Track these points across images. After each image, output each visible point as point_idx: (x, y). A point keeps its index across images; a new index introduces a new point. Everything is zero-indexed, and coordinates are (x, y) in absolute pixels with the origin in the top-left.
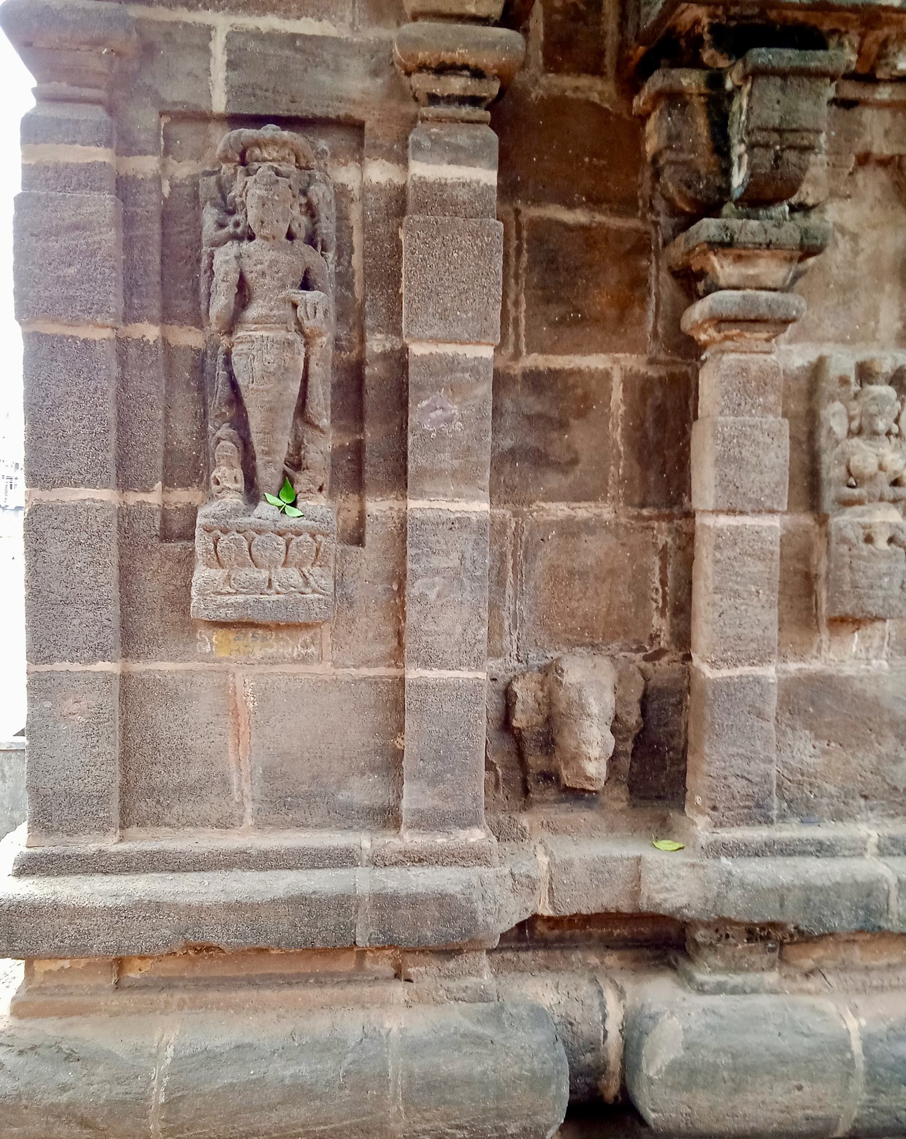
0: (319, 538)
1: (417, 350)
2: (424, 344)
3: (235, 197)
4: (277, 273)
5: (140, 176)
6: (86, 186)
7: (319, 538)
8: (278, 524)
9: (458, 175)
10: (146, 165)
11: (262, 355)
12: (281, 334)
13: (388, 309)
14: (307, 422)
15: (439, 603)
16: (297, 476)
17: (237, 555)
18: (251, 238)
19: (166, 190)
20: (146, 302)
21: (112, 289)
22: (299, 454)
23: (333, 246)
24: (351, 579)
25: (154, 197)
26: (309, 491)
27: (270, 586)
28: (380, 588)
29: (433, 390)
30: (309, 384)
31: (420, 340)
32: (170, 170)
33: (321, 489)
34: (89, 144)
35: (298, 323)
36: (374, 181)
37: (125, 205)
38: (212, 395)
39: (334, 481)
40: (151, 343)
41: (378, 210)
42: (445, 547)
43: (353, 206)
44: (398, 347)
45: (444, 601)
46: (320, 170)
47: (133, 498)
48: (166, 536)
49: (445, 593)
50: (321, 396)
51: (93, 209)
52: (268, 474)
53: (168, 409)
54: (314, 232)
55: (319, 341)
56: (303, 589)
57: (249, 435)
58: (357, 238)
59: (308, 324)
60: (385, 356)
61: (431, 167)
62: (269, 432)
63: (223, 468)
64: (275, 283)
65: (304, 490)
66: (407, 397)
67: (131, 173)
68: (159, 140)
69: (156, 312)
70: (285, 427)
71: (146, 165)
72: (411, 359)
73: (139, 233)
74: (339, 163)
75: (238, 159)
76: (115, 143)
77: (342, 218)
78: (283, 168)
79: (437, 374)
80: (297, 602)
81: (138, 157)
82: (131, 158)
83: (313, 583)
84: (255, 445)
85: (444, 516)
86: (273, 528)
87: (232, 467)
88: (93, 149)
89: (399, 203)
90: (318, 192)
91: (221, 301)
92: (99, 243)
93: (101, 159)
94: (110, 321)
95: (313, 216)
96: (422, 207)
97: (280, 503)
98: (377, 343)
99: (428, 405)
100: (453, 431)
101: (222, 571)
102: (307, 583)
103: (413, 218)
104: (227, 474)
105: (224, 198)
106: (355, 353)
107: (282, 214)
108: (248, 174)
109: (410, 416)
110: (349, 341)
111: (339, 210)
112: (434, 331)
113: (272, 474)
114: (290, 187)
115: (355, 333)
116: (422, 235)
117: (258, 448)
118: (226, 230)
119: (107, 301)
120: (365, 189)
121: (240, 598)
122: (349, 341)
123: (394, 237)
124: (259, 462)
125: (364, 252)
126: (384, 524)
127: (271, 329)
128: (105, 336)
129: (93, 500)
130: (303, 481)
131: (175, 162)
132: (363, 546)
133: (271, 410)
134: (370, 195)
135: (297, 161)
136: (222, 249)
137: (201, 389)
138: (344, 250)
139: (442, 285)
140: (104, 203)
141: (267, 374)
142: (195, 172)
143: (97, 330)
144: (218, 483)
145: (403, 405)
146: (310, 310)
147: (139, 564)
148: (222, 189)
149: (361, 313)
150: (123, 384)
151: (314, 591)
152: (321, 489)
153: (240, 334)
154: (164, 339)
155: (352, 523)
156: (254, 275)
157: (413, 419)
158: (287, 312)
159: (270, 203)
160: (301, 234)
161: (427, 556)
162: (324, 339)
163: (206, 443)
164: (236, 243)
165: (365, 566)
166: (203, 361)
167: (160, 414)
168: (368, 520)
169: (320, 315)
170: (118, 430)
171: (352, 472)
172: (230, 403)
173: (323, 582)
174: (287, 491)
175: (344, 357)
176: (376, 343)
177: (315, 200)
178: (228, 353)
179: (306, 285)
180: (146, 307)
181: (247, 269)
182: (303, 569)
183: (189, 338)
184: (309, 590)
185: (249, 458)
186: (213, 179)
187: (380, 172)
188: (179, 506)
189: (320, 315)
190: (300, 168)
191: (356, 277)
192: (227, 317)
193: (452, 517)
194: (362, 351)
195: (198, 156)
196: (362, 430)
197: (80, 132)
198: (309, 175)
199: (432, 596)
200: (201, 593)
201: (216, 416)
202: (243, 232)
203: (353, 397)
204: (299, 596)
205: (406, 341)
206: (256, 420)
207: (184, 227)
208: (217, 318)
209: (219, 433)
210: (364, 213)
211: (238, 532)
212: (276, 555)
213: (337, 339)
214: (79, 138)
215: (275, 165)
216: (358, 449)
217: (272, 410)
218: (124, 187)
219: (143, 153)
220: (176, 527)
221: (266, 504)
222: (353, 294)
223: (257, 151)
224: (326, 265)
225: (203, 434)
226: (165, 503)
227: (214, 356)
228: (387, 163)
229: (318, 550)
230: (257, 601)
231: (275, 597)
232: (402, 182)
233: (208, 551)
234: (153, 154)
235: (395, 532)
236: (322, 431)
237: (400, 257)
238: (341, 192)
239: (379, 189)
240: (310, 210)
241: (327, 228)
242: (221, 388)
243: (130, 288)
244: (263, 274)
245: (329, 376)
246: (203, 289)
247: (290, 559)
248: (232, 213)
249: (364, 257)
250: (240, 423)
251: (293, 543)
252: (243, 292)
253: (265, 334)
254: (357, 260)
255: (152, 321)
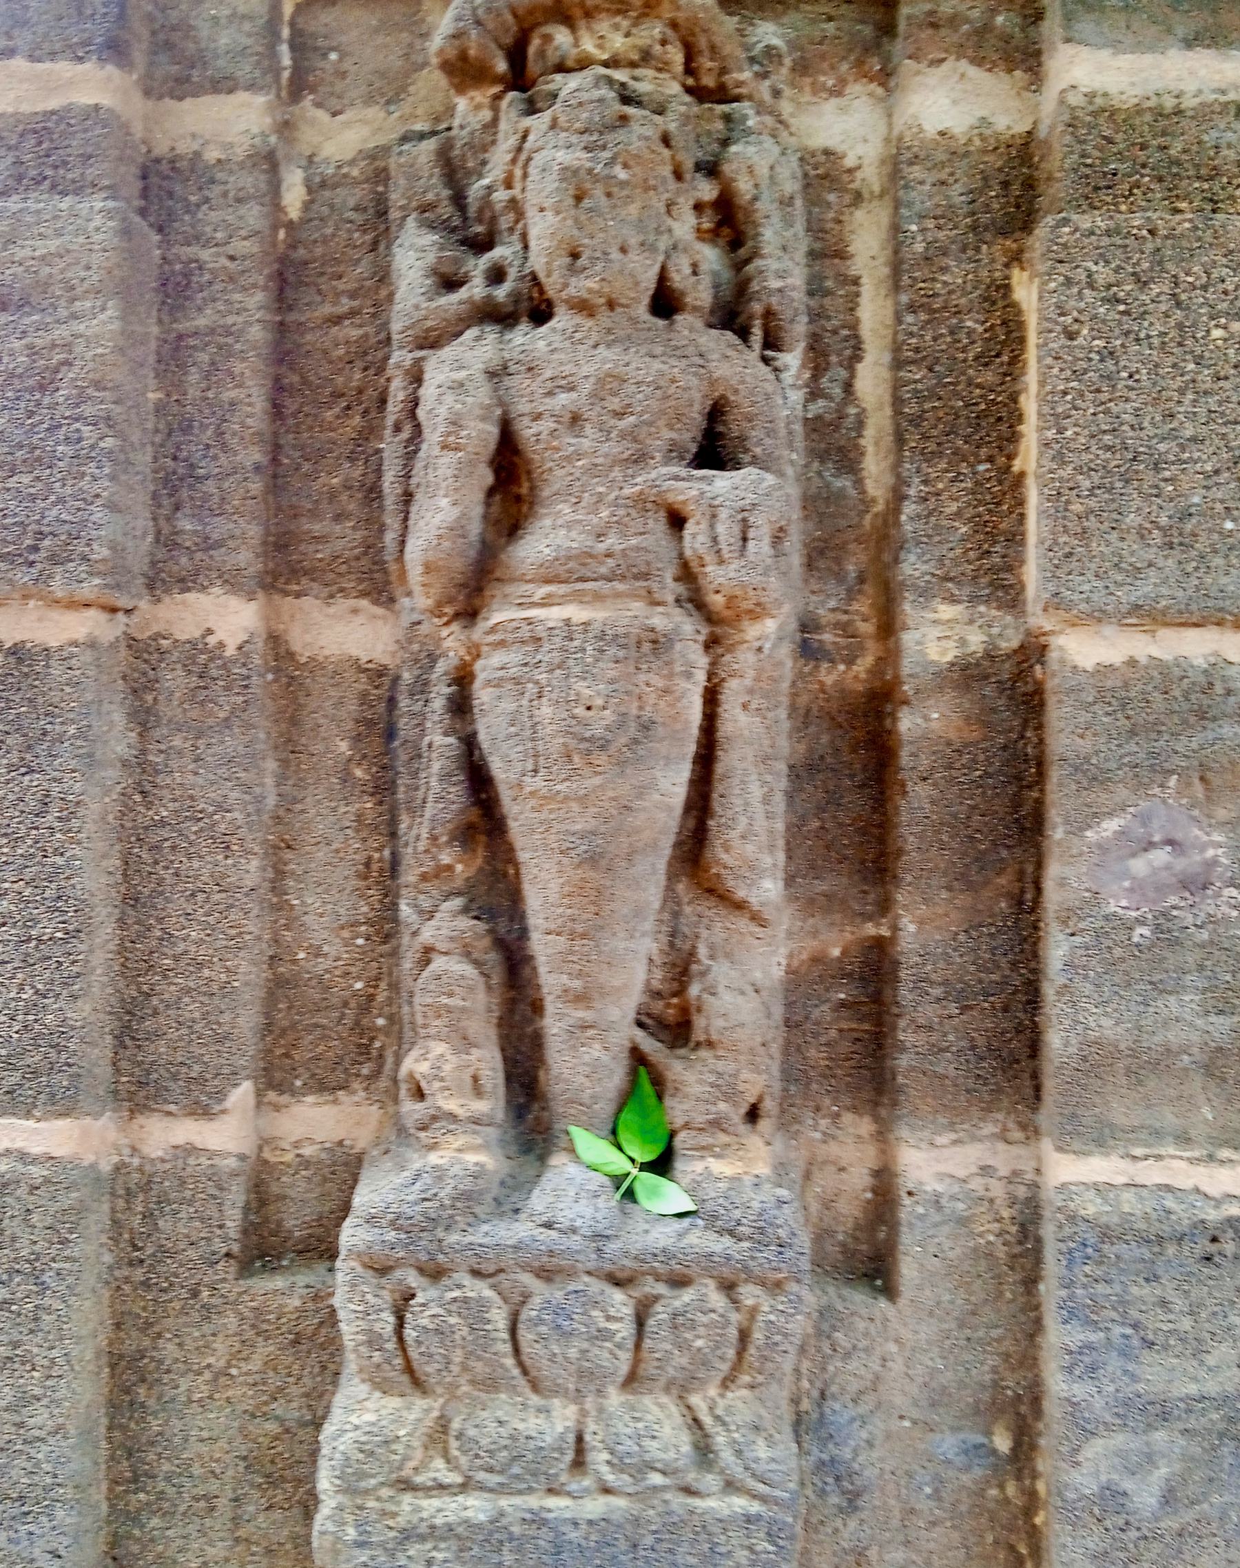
0: (750, 1294)
1: (1082, 650)
2: (1109, 630)
3: (490, 189)
4: (620, 415)
5: (211, 155)
6: (39, 181)
7: (750, 1294)
8: (612, 1247)
9: (1217, 81)
10: (231, 122)
11: (568, 681)
12: (629, 613)
13: (979, 525)
14: (710, 891)
15: (1171, 1523)
16: (676, 1068)
17: (469, 1355)
18: (541, 314)
19: (294, 197)
20: (219, 528)
21: (105, 488)
22: (680, 992)
23: (799, 329)
24: (852, 1412)
25: (253, 215)
26: (717, 1124)
27: (579, 1463)
28: (948, 1444)
29: (1140, 786)
30: (719, 768)
31: (1096, 617)
32: (307, 138)
33: (753, 1115)
34: (53, 56)
35: (687, 574)
36: (931, 128)
37: (166, 243)
38: (412, 811)
39: (794, 1075)
40: (230, 651)
41: (943, 217)
42: (1186, 1324)
43: (859, 215)
44: (1010, 642)
45: (1188, 1516)
46: (761, 109)
47: (163, 1134)
48: (262, 1249)
49: (1193, 1490)
50: (758, 809)
51: (53, 245)
52: (583, 1063)
53: (281, 851)
54: (741, 290)
55: (752, 631)
56: (691, 1477)
57: (524, 934)
58: (874, 313)
59: (719, 578)
60: (966, 675)
61: (1126, 61)
62: (582, 935)
63: (439, 1048)
64: (613, 448)
65: (700, 1119)
66: (1039, 804)
67: (185, 147)
68: (272, 54)
69: (246, 558)
70: (638, 913)
71: (231, 122)
72: (1054, 680)
73: (201, 322)
74: (817, 89)
75: (501, 66)
76: (139, 55)
77: (827, 252)
78: (646, 83)
79: (1155, 728)
80: (673, 1526)
81: (207, 99)
82: (188, 103)
83: (726, 1456)
84: (542, 970)
85: (1182, 1214)
86: (591, 1261)
87: (466, 1043)
88: (64, 68)
89: (1011, 192)
90: (758, 165)
91: (442, 511)
92: (68, 347)
93: (86, 99)
94: (90, 588)
95: (736, 243)
96: (1097, 187)
97: (620, 1164)
98: (939, 635)
99: (1122, 833)
100: (1211, 920)
101: (420, 1403)
102: (704, 1452)
103: (1059, 227)
104: (451, 1062)
105: (459, 200)
106: (865, 663)
107: (640, 225)
108: (532, 109)
109: (1054, 871)
110: (845, 629)
111: (815, 229)
112: (1145, 589)
113: (595, 1066)
114: (666, 140)
115: (862, 606)
116: (1103, 274)
117: (551, 979)
118: (463, 293)
119: (83, 523)
120: (899, 161)
121: (476, 1507)
122: (845, 629)
123: (998, 296)
124: (554, 1024)
125: (897, 349)
126: (963, 1221)
127: (598, 597)
128: (80, 633)
129: (23, 1157)
130: (696, 1089)
131: (322, 115)
132: (889, 1291)
133: (592, 860)
134: (916, 172)
135: (689, 70)
136: (447, 352)
137: (383, 788)
138: (832, 351)
139: (1171, 435)
140: (86, 227)
141: (588, 747)
142: (381, 140)
143: (56, 615)
144: (420, 1094)
145: (1025, 828)
146: (726, 530)
147: (169, 1349)
148: (454, 173)
149: (885, 541)
150: (143, 778)
151: (731, 1486)
152: (753, 1115)
153: (497, 618)
154: (274, 640)
155: (850, 1210)
156: (546, 425)
157: (1064, 878)
158: (647, 541)
159: (598, 192)
160: (700, 294)
161: (1124, 1354)
162: (770, 626)
163: (395, 953)
164: (491, 333)
165: (897, 1366)
166: (392, 702)
167: (252, 871)
168: (908, 1210)
169: (760, 547)
170: (122, 922)
171: (855, 1039)
172: (466, 835)
173: (762, 1451)
174: (644, 1114)
175: (829, 680)
176: (936, 632)
177: (744, 186)
178: (463, 679)
179: (714, 449)
180: (219, 544)
181: (523, 407)
182: (695, 1400)
183: (346, 633)
184: (711, 1481)
185: (524, 1008)
186: (430, 145)
187: (949, 102)
188: (307, 1151)
189: (760, 547)
190: (698, 93)
191: (870, 432)
192: (460, 565)
193: (1212, 1215)
194: (890, 656)
195: (390, 91)
196: (884, 906)
197: (25, 23)
198: (727, 118)
199: (1145, 1496)
200: (350, 1487)
201: (424, 877)
202: (516, 297)
203: (855, 803)
204: (678, 1502)
205: (1038, 619)
206: (544, 892)
207: (346, 304)
208: (428, 568)
209: (428, 934)
210: (896, 229)
211: (476, 1273)
212: (602, 1354)
213: (807, 625)
214: (23, 39)
215: (620, 75)
216: (875, 969)
217: (596, 860)
218: (162, 188)
219: (223, 85)
220: (295, 1220)
221: (572, 1169)
222: (859, 483)
223: (562, 36)
224: (777, 393)
225: (385, 927)
226: (265, 1142)
227: (422, 687)
228: (973, 71)
229: (744, 1336)
230: (537, 1520)
231: (595, 1506)
232: (1022, 127)
233: (374, 1340)
234: (251, 87)
235: (1001, 1252)
236: (756, 918)
237: (1016, 360)
238: (824, 176)
239: (949, 151)
240: (729, 222)
241: (782, 270)
242: (436, 796)
243: (174, 485)
244: (576, 419)
245: (784, 744)
246: (390, 483)
247: (649, 1368)
248: (482, 245)
249: (898, 364)
250: (497, 899)
251: (661, 1313)
252: (510, 480)
253: (576, 613)
254: (872, 381)
255: (233, 582)
